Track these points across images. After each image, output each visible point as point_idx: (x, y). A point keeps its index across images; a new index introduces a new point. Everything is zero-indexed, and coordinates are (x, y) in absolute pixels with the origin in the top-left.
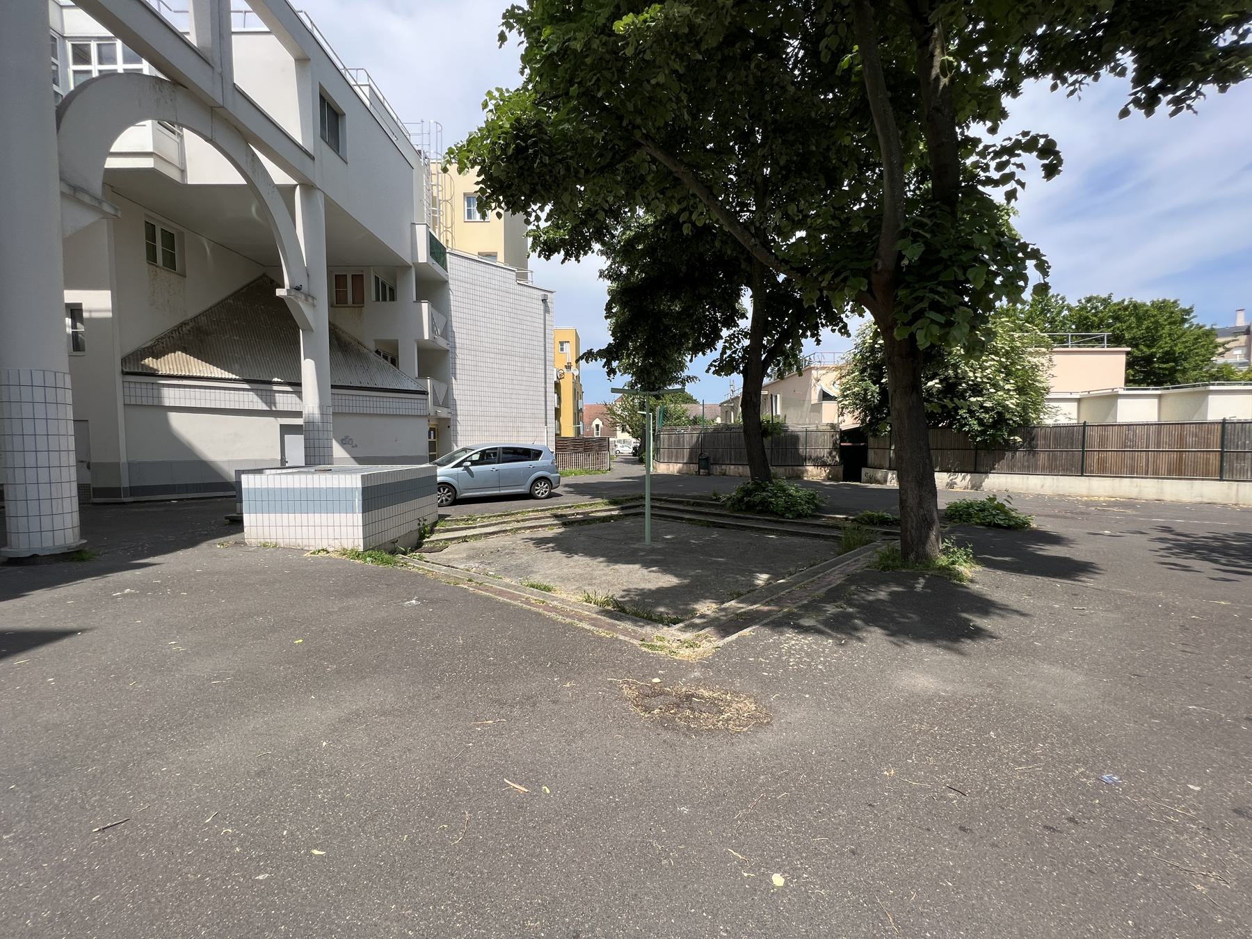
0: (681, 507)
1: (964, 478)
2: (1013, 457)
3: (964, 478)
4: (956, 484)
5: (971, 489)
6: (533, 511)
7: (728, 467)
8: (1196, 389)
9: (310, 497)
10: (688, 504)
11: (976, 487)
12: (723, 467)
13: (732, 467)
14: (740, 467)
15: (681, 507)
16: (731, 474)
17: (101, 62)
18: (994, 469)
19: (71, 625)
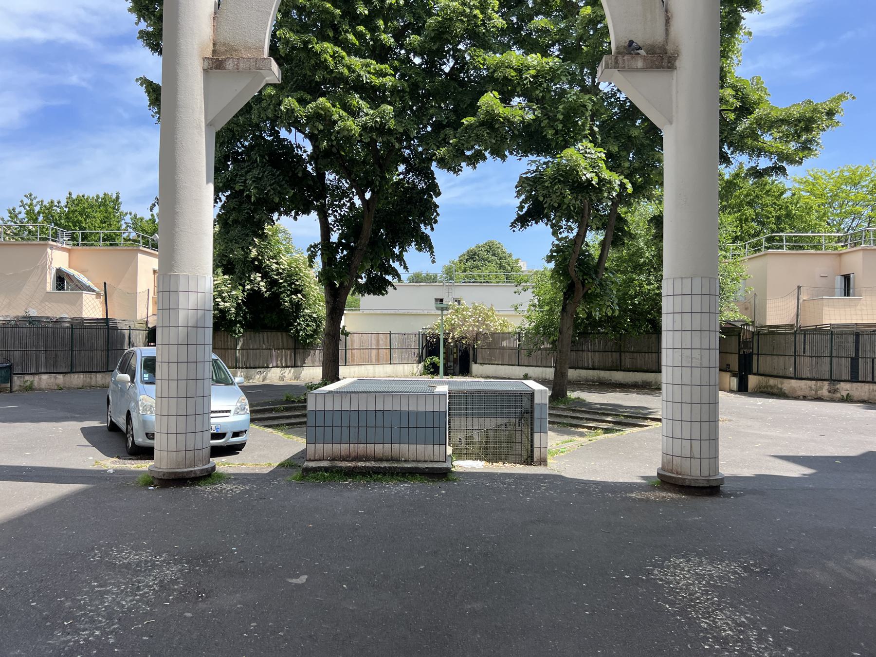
0: (273, 415)
1: (290, 372)
2: (314, 354)
3: (290, 372)
4: (285, 377)
5: (294, 380)
6: (804, 345)
7: (37, 377)
8: (354, 312)
9: (421, 424)
10: (277, 410)
11: (297, 378)
12: (27, 378)
13: (44, 377)
14: (60, 377)
15: (273, 415)
16: (43, 387)
17: (786, 242)
18: (305, 363)
19: (773, 459)
